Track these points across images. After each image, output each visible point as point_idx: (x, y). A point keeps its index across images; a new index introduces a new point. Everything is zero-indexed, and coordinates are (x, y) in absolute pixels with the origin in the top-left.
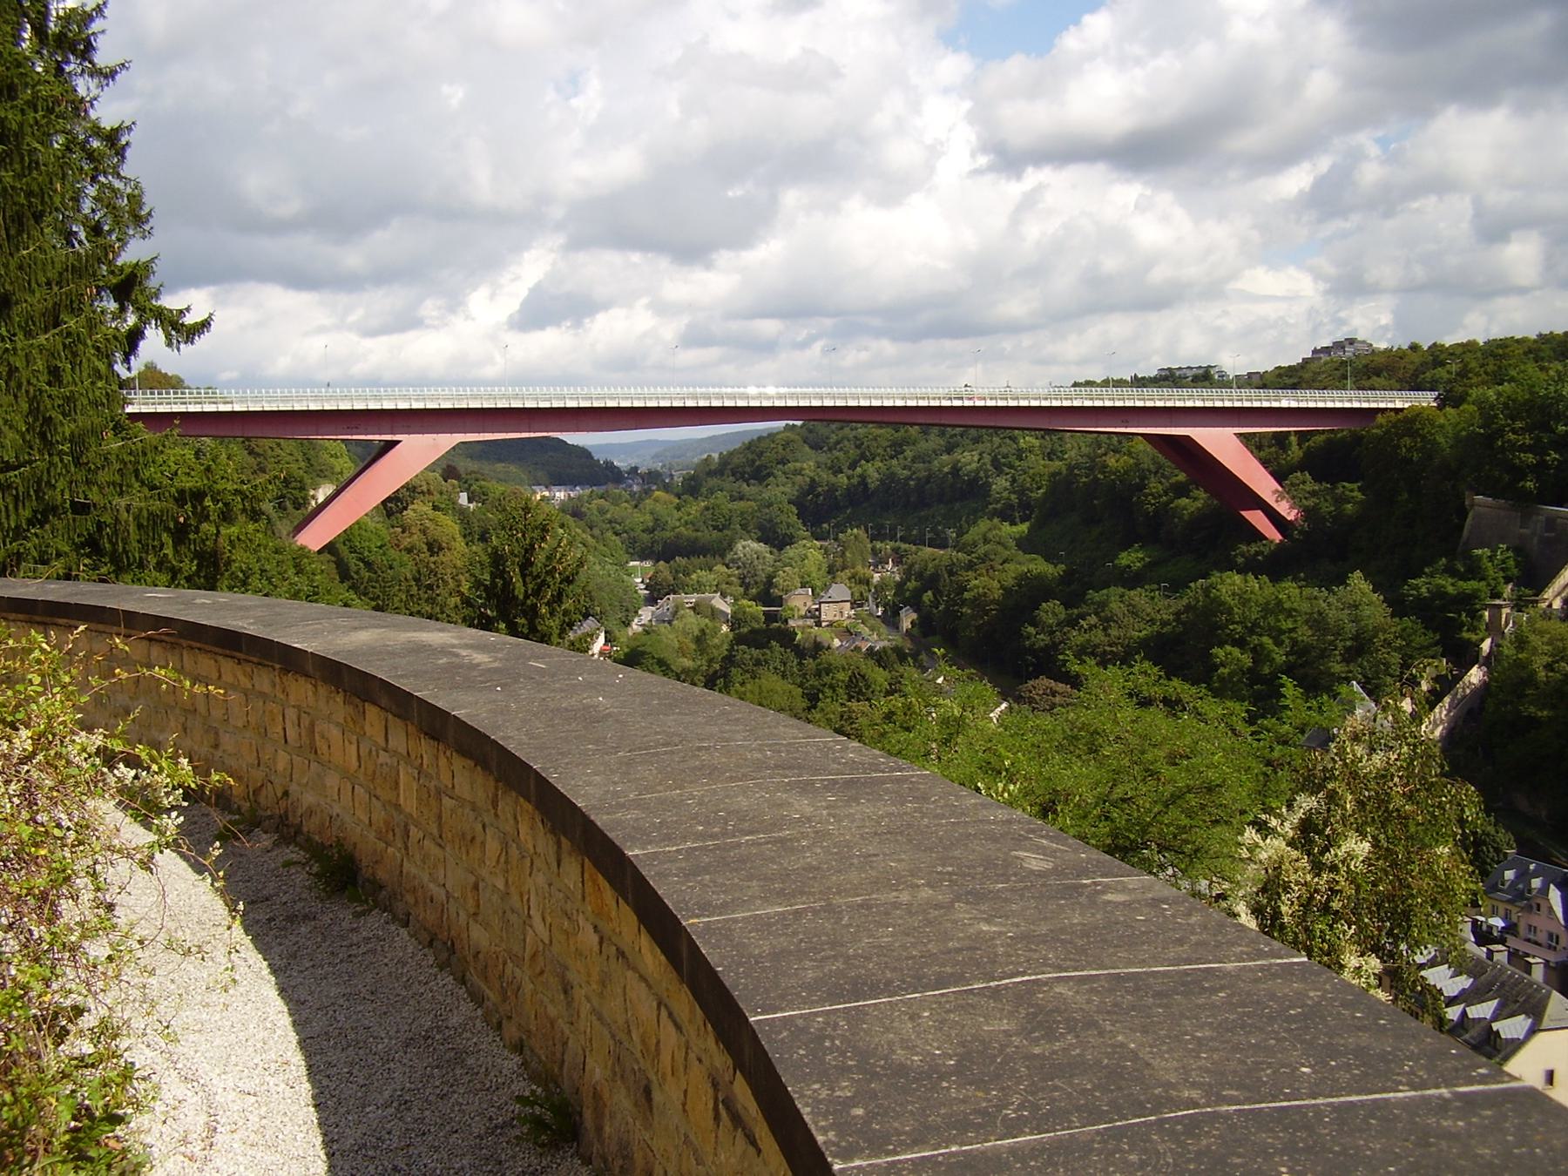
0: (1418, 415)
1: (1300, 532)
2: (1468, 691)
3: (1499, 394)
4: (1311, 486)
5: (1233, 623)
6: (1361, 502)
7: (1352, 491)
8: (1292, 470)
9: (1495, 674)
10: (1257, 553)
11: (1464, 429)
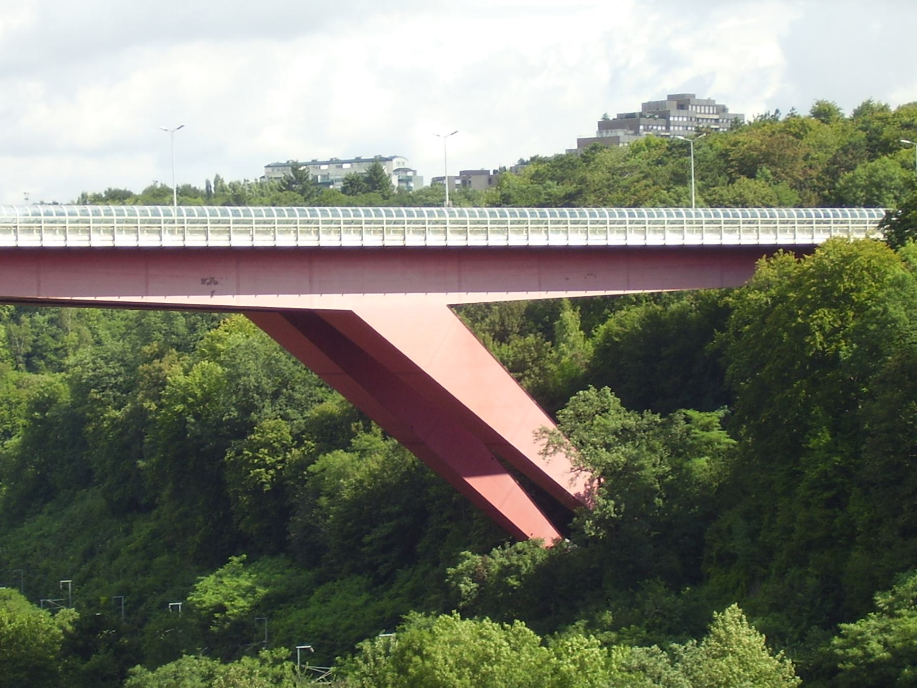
0: (846, 260)
7: (707, 428)
8: (577, 384)
10: (506, 571)
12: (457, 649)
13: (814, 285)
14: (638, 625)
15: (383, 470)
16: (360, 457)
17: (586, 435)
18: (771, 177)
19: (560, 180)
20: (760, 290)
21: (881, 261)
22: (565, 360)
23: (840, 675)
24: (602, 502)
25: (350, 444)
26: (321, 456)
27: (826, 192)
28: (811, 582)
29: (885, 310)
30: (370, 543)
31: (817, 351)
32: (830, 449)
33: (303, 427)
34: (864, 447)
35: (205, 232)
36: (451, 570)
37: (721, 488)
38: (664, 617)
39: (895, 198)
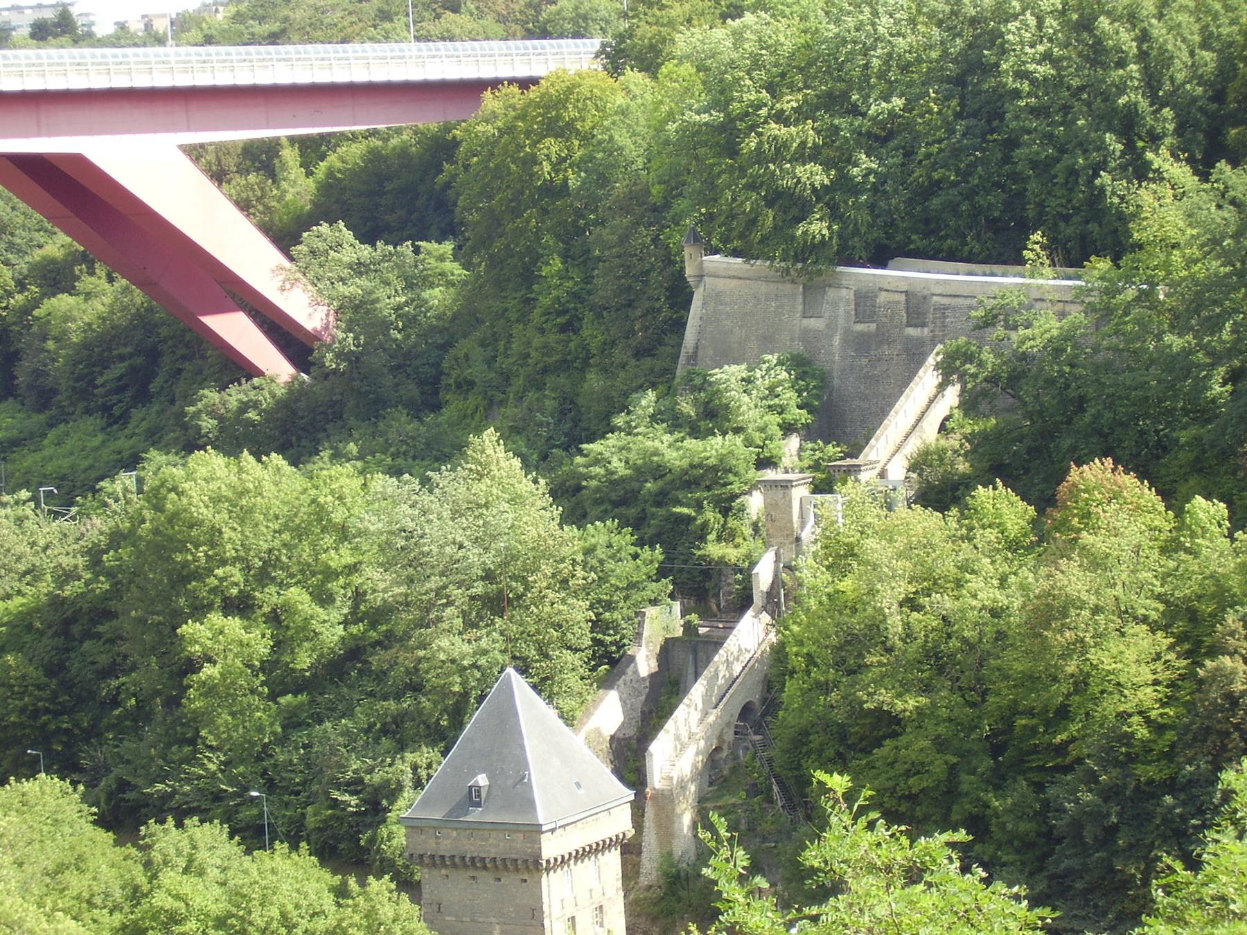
0: (569, 90)
1: (340, 355)
2: (737, 668)
3: (738, 37)
4: (353, 250)
5: (223, 562)
6: (465, 283)
7: (441, 258)
8: (306, 222)
9: (795, 628)
10: (244, 407)
11: (671, 116)
12: (213, 486)
13: (539, 115)
14: (384, 453)
15: (112, 312)
16: (86, 300)
17: (321, 271)
18: (476, 12)
19: (262, 19)
20: (487, 122)
21: (603, 91)
22: (289, 197)
23: (584, 492)
24: (341, 335)
25: (74, 287)
26: (45, 300)
27: (531, 25)
28: (549, 404)
29: (611, 138)
30: (103, 385)
31: (545, 180)
32: (563, 275)
33: (25, 272)
34: (596, 272)
35: (129, 72)
36: (192, 409)
37: (455, 317)
38: (408, 444)
39: (601, 29)
